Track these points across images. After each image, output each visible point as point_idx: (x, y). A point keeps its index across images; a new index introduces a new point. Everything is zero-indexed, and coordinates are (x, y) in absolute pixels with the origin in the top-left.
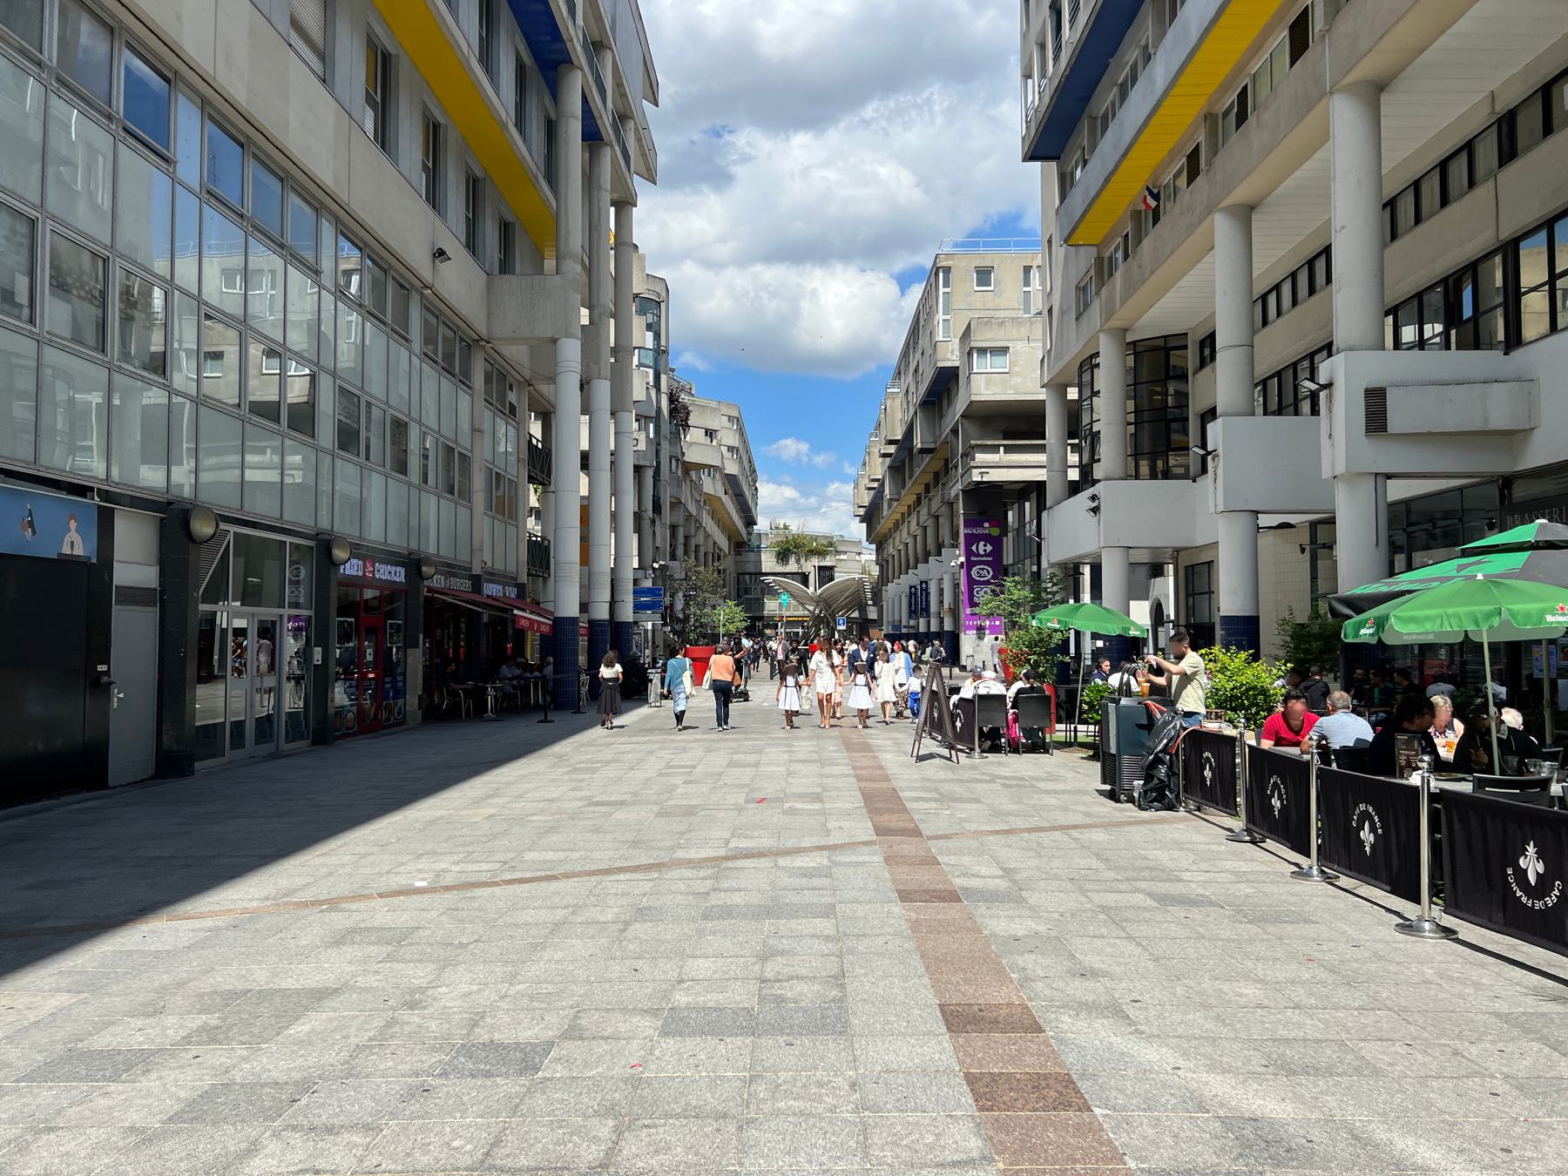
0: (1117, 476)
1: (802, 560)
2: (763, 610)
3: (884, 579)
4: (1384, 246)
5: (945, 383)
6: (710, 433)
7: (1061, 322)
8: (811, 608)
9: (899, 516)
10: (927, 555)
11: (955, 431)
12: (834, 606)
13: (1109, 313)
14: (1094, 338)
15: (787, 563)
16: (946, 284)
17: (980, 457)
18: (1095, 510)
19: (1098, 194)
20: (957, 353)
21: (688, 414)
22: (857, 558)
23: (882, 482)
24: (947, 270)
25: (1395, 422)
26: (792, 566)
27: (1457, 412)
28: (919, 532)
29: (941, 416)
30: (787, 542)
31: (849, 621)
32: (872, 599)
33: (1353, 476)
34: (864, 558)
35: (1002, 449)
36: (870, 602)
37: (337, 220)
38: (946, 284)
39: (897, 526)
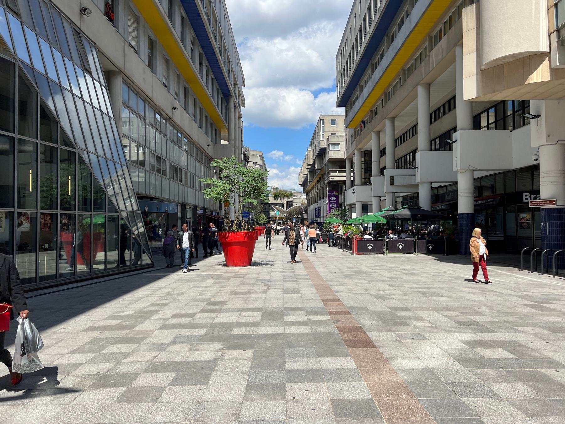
0: (359, 184)
1: (282, 199)
2: (270, 215)
3: (309, 205)
4: (394, 148)
5: (322, 153)
6: (255, 163)
7: (348, 143)
8: (285, 215)
9: (313, 186)
10: (320, 199)
11: (326, 165)
12: (293, 214)
13: (357, 146)
14: (354, 151)
15: (277, 200)
16: (323, 124)
17: (332, 174)
18: (354, 193)
19: (354, 117)
20: (326, 144)
21: (249, 158)
22: (300, 198)
23: (307, 175)
24: (323, 120)
25: (396, 182)
26: (279, 201)
27: (406, 181)
28: (318, 191)
29: (323, 160)
30: (277, 193)
31: (297, 218)
32: (304, 212)
33: (388, 193)
34: (302, 197)
35: (338, 172)
36: (304, 213)
37: (149, 103)
38: (323, 124)
39: (312, 188)
